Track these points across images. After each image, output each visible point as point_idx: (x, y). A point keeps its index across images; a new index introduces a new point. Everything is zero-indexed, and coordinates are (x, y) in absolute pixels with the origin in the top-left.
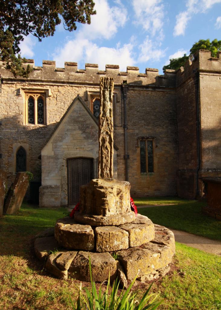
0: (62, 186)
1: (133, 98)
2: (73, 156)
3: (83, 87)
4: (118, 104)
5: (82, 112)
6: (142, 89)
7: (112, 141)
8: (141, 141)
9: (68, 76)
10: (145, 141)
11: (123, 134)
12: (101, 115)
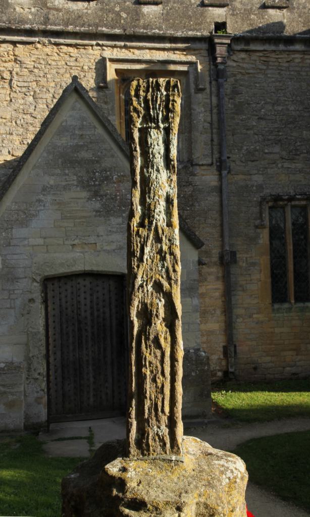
0: (30, 365)
1: (246, 77)
2: (62, 270)
3: (92, 46)
4: (200, 96)
5: (89, 133)
6: (273, 48)
7: (177, 317)
8: (270, 208)
9: (45, 11)
10: (283, 207)
11: (216, 187)
12: (136, 221)
